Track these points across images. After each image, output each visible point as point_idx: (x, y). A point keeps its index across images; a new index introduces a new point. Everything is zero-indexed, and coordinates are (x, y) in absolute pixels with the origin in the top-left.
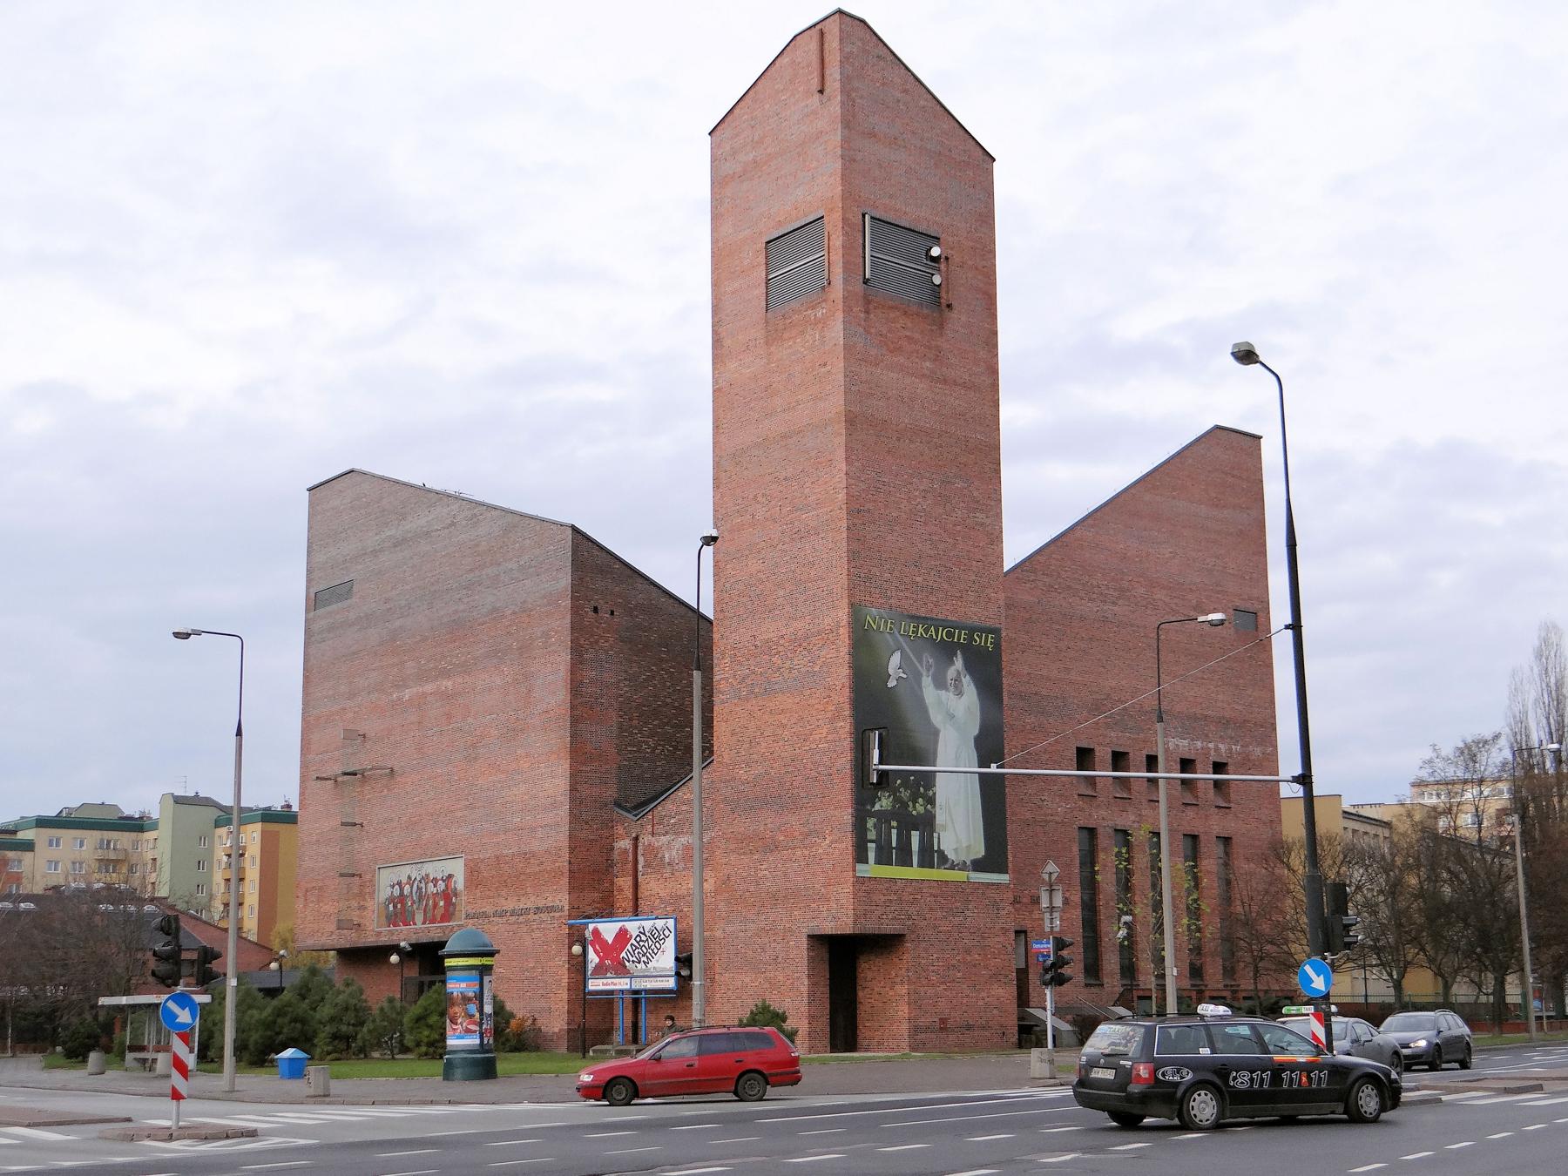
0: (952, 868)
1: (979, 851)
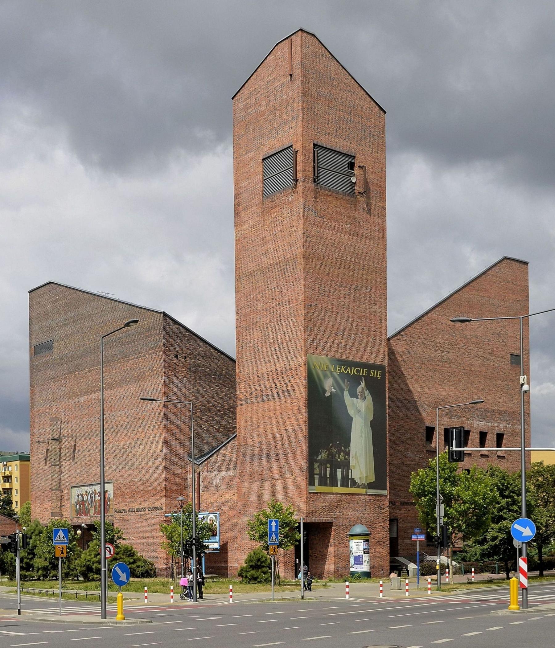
0: (358, 487)
1: (372, 479)
